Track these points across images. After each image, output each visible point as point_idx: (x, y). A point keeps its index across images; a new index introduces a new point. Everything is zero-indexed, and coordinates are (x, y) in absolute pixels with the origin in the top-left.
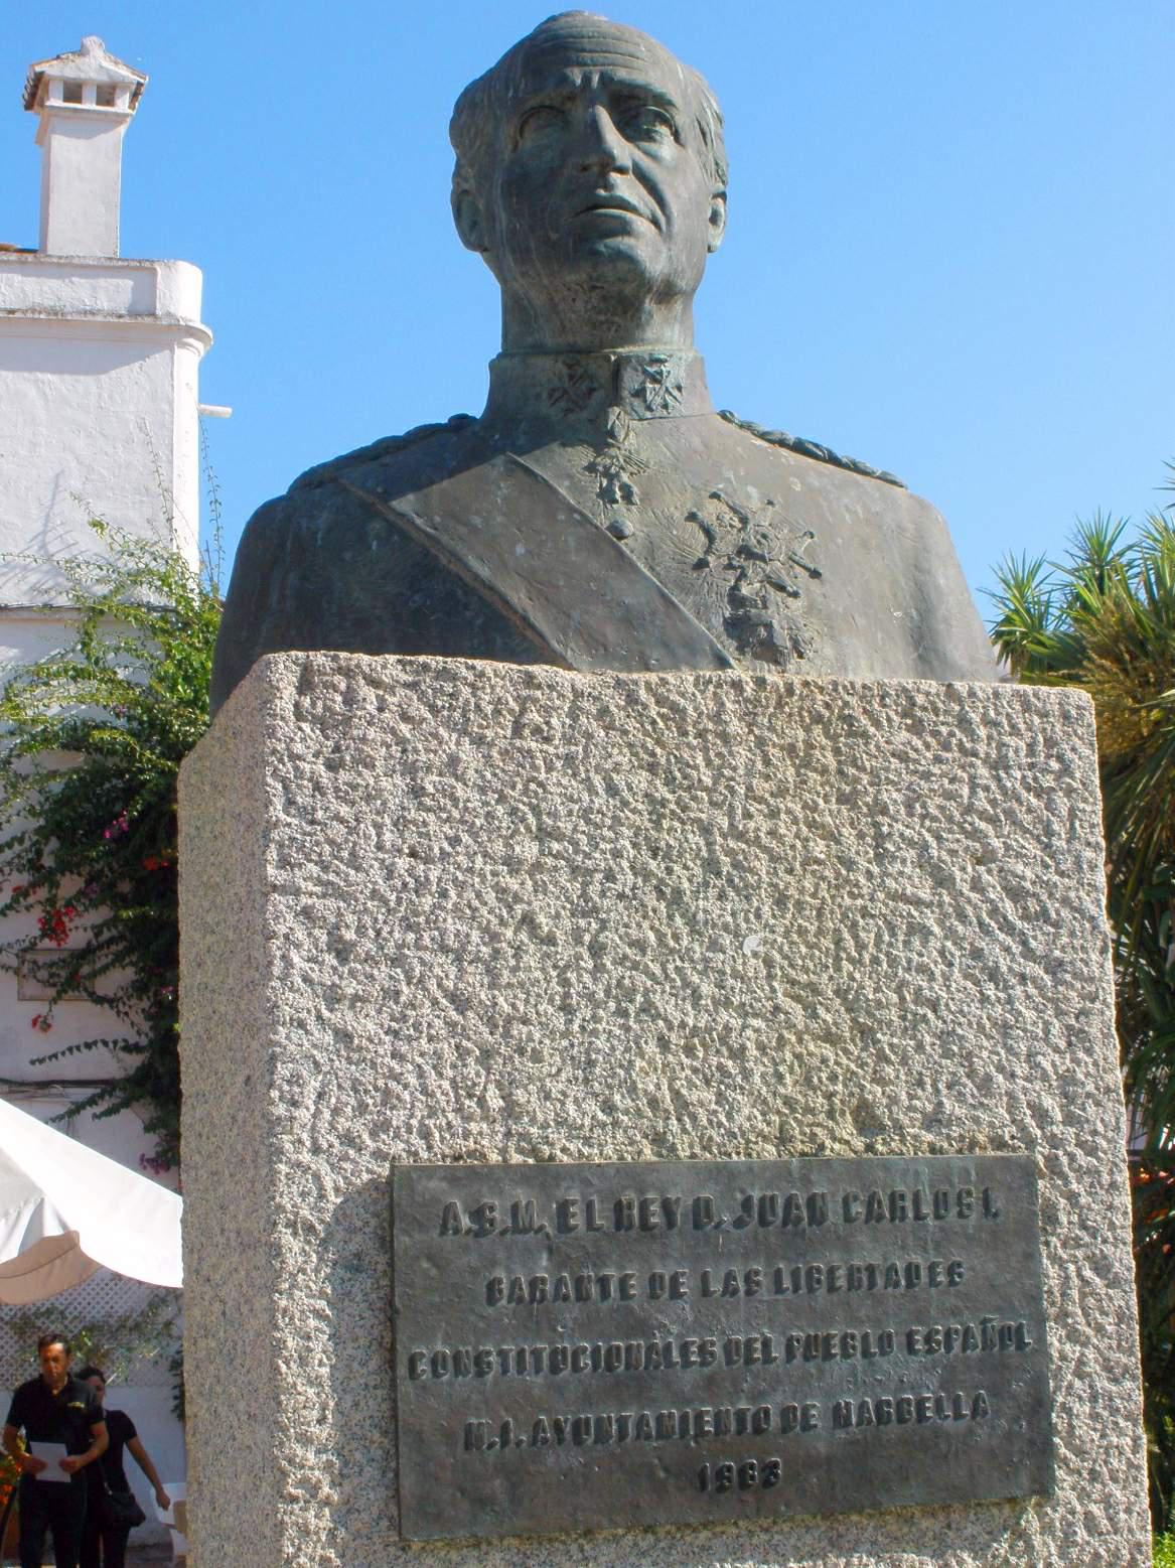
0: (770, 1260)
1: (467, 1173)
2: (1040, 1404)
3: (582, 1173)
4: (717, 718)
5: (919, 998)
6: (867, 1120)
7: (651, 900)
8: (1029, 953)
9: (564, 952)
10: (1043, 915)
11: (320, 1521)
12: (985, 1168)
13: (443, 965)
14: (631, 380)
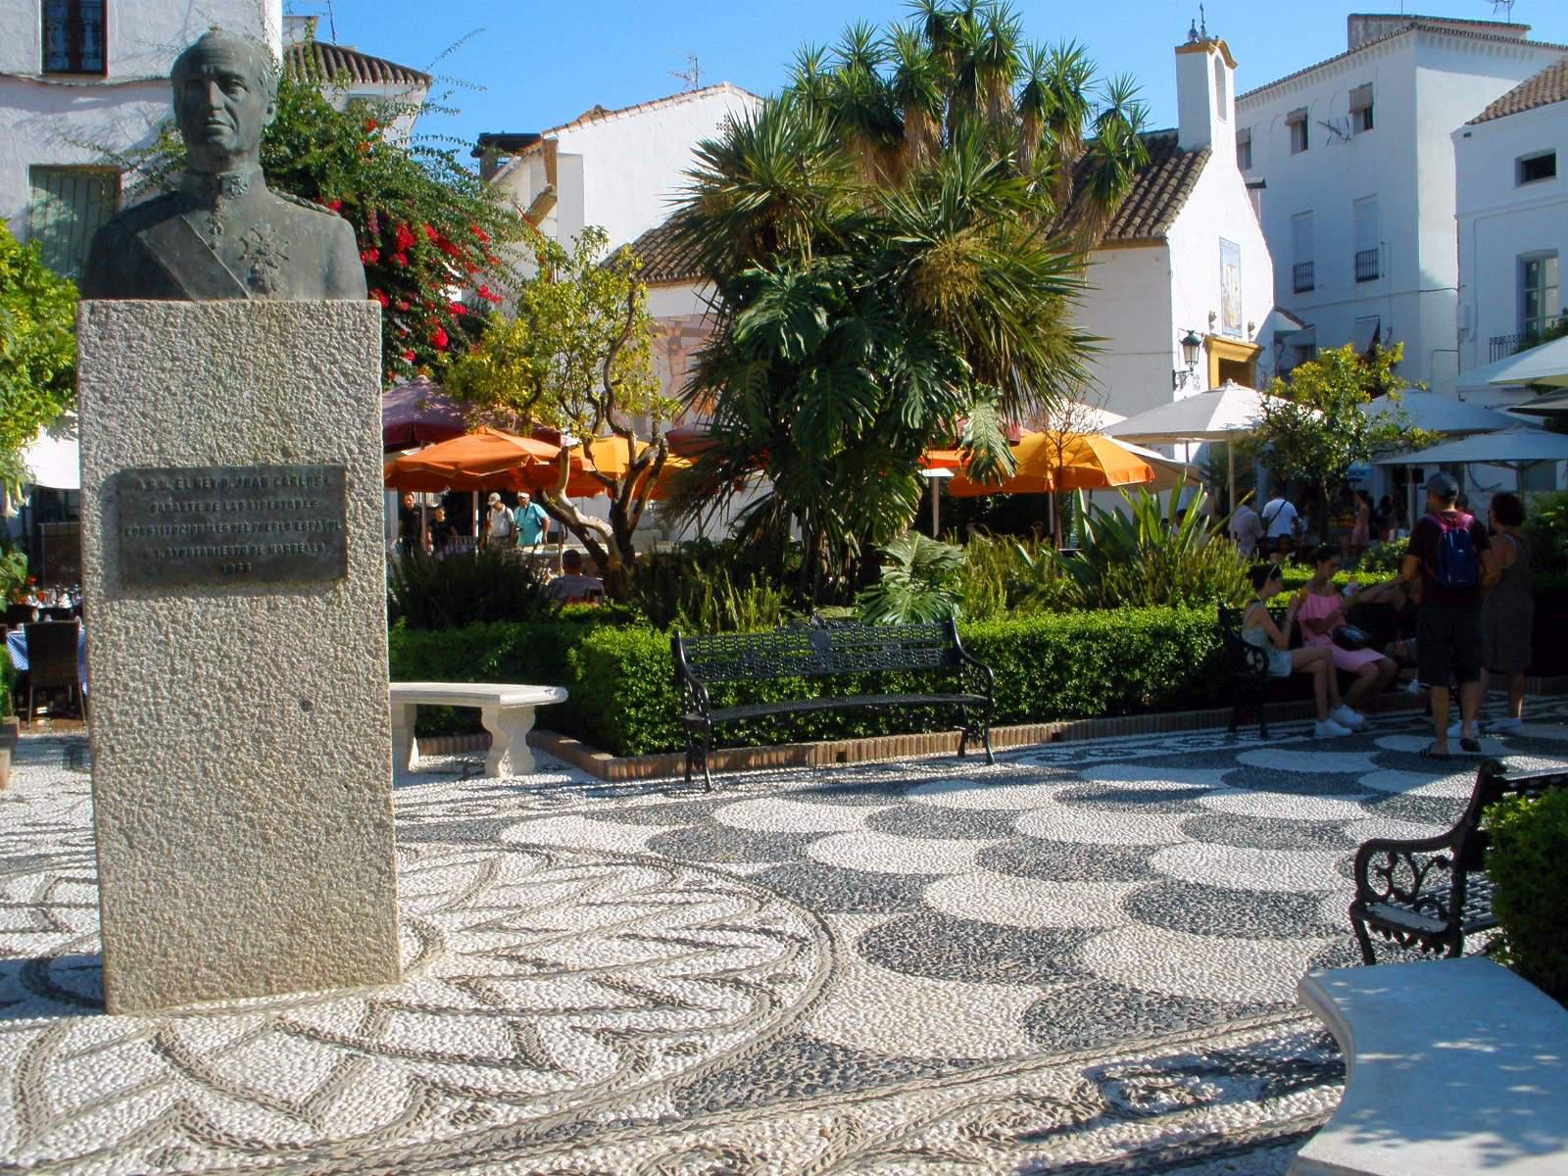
0: (248, 498)
1: (146, 472)
2: (343, 547)
3: (184, 471)
4: (236, 317)
5: (306, 411)
6: (286, 452)
7: (211, 380)
8: (348, 395)
9: (179, 399)
10: (355, 382)
11: (97, 580)
12: (327, 470)
13: (138, 404)
14: (226, 185)
